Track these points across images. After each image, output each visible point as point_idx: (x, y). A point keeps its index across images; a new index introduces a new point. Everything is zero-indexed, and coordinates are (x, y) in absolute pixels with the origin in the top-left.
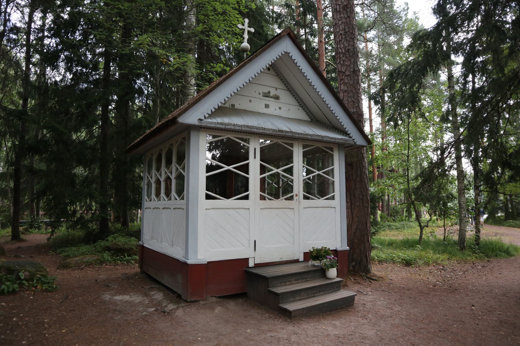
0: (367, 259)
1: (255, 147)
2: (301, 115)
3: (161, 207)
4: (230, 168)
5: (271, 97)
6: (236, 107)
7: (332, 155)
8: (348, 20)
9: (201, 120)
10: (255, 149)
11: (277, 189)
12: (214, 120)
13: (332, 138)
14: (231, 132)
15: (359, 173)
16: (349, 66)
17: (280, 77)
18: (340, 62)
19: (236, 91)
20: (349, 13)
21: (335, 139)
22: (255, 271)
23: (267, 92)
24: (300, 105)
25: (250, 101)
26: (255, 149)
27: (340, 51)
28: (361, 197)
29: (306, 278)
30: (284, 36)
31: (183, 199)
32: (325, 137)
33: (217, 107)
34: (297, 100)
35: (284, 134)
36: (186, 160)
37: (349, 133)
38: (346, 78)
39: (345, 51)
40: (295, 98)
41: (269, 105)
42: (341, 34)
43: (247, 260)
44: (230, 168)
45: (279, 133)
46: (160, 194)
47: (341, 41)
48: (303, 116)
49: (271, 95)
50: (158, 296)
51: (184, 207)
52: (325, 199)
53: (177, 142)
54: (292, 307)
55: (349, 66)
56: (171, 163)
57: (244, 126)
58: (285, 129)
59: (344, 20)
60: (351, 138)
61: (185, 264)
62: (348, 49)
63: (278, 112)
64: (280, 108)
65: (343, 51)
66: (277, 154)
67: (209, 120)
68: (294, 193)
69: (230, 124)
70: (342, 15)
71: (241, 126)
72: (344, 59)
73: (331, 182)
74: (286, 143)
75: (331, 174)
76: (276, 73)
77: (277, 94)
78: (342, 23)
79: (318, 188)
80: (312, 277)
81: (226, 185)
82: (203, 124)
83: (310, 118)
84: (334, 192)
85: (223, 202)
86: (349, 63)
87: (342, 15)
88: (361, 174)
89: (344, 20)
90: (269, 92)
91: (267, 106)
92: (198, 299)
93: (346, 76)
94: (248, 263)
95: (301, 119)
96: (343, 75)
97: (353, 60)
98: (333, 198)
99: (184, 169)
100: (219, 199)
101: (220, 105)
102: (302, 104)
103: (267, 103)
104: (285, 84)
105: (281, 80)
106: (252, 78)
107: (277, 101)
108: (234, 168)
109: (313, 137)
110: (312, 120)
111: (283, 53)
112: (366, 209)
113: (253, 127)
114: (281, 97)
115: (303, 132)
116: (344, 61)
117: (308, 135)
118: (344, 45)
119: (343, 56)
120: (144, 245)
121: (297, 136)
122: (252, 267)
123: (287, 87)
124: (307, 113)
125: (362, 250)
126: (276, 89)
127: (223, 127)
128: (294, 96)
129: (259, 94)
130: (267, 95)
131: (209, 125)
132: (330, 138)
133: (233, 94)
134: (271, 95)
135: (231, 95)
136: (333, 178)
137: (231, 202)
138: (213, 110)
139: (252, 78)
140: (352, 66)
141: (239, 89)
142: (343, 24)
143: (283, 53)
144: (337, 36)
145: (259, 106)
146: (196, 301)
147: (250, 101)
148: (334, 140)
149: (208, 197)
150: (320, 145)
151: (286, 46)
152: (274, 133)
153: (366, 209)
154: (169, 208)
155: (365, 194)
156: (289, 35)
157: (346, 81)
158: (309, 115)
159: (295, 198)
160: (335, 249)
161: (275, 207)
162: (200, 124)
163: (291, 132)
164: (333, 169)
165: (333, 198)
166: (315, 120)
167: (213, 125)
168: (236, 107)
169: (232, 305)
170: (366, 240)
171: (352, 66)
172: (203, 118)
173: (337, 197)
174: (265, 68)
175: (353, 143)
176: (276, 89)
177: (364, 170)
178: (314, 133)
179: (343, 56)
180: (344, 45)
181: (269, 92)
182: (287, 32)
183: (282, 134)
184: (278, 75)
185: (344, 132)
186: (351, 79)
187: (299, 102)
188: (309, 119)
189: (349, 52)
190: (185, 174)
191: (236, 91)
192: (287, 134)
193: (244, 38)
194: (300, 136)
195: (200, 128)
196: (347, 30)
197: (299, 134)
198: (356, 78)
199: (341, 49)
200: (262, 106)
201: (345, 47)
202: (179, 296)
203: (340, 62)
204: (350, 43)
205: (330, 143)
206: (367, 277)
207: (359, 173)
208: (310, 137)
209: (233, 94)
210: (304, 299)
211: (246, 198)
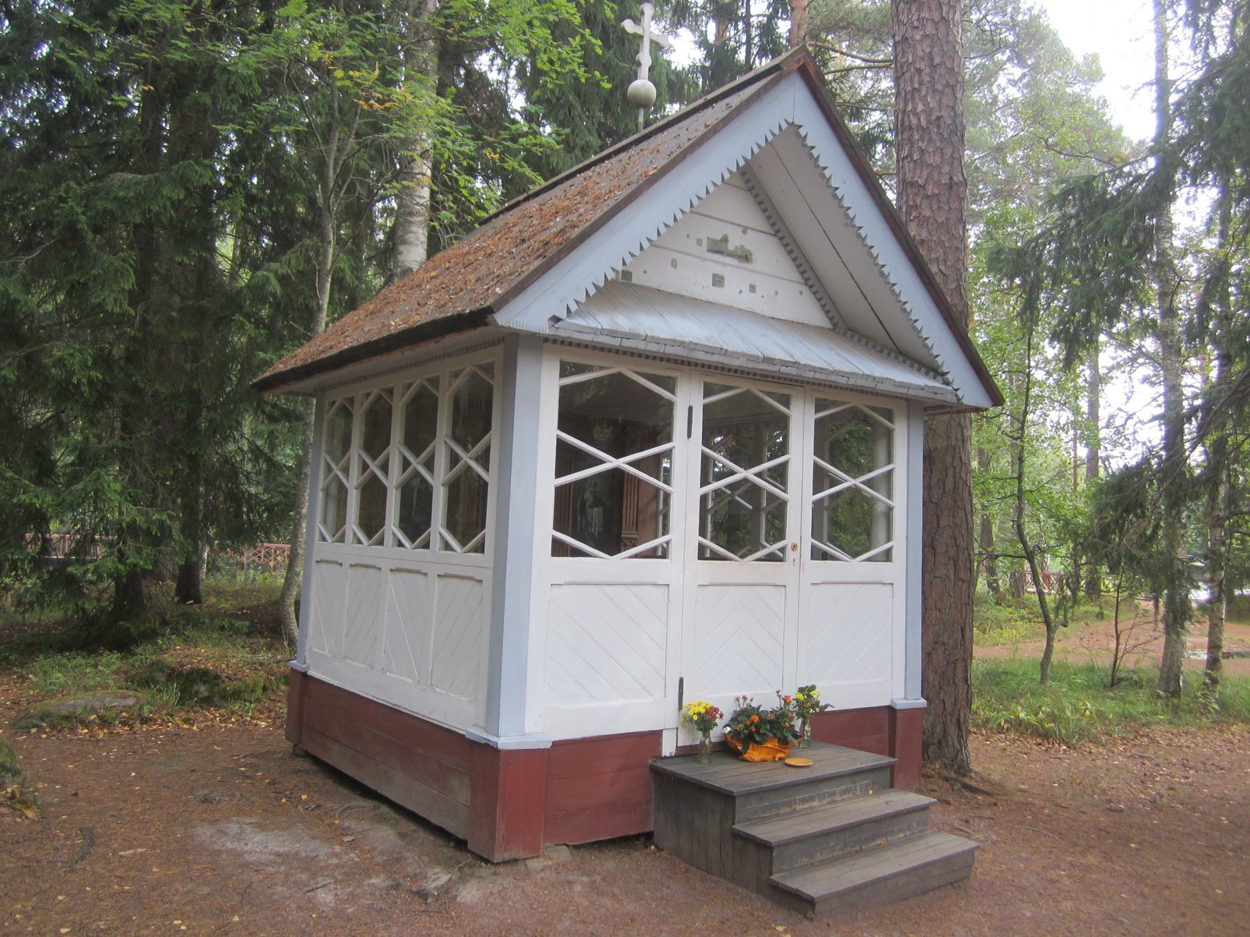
0: (960, 729)
1: (688, 402)
2: (806, 309)
3: (386, 566)
4: (622, 463)
5: (730, 255)
6: (634, 281)
7: (889, 434)
8: (942, 28)
9: (556, 319)
10: (690, 409)
11: (739, 526)
12: (590, 323)
13: (902, 385)
14: (627, 357)
15: (949, 486)
16: (938, 167)
17: (756, 196)
18: (910, 155)
19: (654, 237)
20: (945, 8)
21: (909, 386)
22: (686, 770)
23: (719, 237)
24: (807, 280)
25: (674, 264)
26: (690, 409)
27: (914, 121)
28: (952, 552)
29: (834, 794)
30: (789, 73)
31: (480, 548)
32: (882, 380)
33: (601, 284)
34: (798, 266)
35: (776, 368)
36: (494, 436)
37: (945, 369)
38: (925, 203)
39: (929, 122)
40: (794, 260)
41: (723, 278)
42: (919, 71)
43: (656, 735)
44: (622, 463)
45: (764, 366)
46: (381, 523)
47: (918, 90)
48: (811, 313)
49: (731, 247)
50: (385, 835)
51: (487, 576)
52: (869, 560)
53: (457, 374)
54: (815, 884)
55: (938, 167)
56: (433, 435)
57: (674, 343)
58: (779, 354)
59: (929, 29)
60: (948, 384)
61: (487, 750)
62: (938, 118)
63: (745, 301)
64: (752, 288)
65: (924, 123)
66: (745, 425)
67: (579, 321)
68: (788, 542)
69: (635, 336)
70: (925, 14)
71: (665, 342)
72: (923, 145)
73: (880, 508)
74: (769, 394)
75: (883, 487)
76: (747, 181)
77: (748, 247)
78: (925, 36)
79: (848, 527)
80: (847, 791)
81: (605, 517)
82: (563, 333)
83: (831, 319)
84: (889, 538)
85: (599, 564)
86: (938, 159)
87: (925, 14)
88: (955, 487)
89: (929, 29)
90: (725, 240)
91: (718, 281)
92: (519, 854)
93: (928, 197)
94: (660, 744)
95: (806, 321)
96: (916, 194)
97: (948, 151)
98: (887, 556)
99: (484, 459)
100: (595, 557)
101: (611, 276)
102: (810, 277)
103: (720, 270)
104: (769, 218)
105: (760, 203)
106: (699, 198)
107: (744, 265)
108: (632, 464)
109: (852, 381)
110: (835, 325)
111: (784, 126)
112: (965, 585)
113: (694, 346)
114: (756, 255)
115: (825, 366)
116: (922, 151)
117: (838, 373)
118: (926, 104)
119: (922, 139)
120: (311, 673)
121: (810, 375)
122: (671, 757)
123: (773, 225)
124: (823, 306)
125: (949, 707)
126: (745, 232)
127: (615, 342)
128: (790, 252)
129: (699, 242)
130: (718, 247)
131: (577, 336)
132: (894, 383)
133: (646, 245)
134: (731, 247)
135: (642, 248)
136: (890, 496)
137: (621, 564)
138: (592, 291)
139: (699, 198)
140: (946, 169)
141: (663, 230)
142: (928, 41)
143: (784, 126)
144: (907, 76)
145: (693, 277)
146: (516, 860)
147: (674, 264)
148: (905, 391)
149: (559, 549)
150: (861, 403)
151: (792, 104)
152: (751, 365)
153: (965, 585)
154: (418, 572)
155: (963, 545)
156: (803, 72)
157: (927, 213)
158: (827, 313)
159: (790, 554)
160: (888, 703)
161: (736, 581)
162: (553, 332)
163: (796, 364)
164: (890, 473)
165: (887, 556)
166: (844, 327)
167: (587, 338)
168: (634, 281)
169: (609, 863)
170: (960, 675)
171: (946, 169)
172: (562, 314)
173: (899, 554)
174: (734, 170)
175: (954, 400)
176: (745, 232)
177: (963, 475)
178: (856, 370)
179: (922, 139)
180: (926, 104)
181: (725, 240)
182: (799, 60)
183: (771, 368)
184: (750, 190)
185: (933, 370)
186: (939, 208)
187: (802, 273)
188: (826, 324)
189: (939, 127)
190: (490, 477)
191: (654, 237)
192: (783, 369)
193: (639, 64)
194: (818, 376)
195: (539, 343)
196: (937, 60)
197: (814, 369)
198: (954, 205)
199: (917, 115)
200: (686, 273)
201: (928, 112)
202: (461, 844)
203: (910, 155)
204: (944, 100)
205: (887, 396)
206: (965, 786)
207: (949, 486)
208: (843, 381)
209: (646, 245)
210: (836, 859)
211: (661, 553)
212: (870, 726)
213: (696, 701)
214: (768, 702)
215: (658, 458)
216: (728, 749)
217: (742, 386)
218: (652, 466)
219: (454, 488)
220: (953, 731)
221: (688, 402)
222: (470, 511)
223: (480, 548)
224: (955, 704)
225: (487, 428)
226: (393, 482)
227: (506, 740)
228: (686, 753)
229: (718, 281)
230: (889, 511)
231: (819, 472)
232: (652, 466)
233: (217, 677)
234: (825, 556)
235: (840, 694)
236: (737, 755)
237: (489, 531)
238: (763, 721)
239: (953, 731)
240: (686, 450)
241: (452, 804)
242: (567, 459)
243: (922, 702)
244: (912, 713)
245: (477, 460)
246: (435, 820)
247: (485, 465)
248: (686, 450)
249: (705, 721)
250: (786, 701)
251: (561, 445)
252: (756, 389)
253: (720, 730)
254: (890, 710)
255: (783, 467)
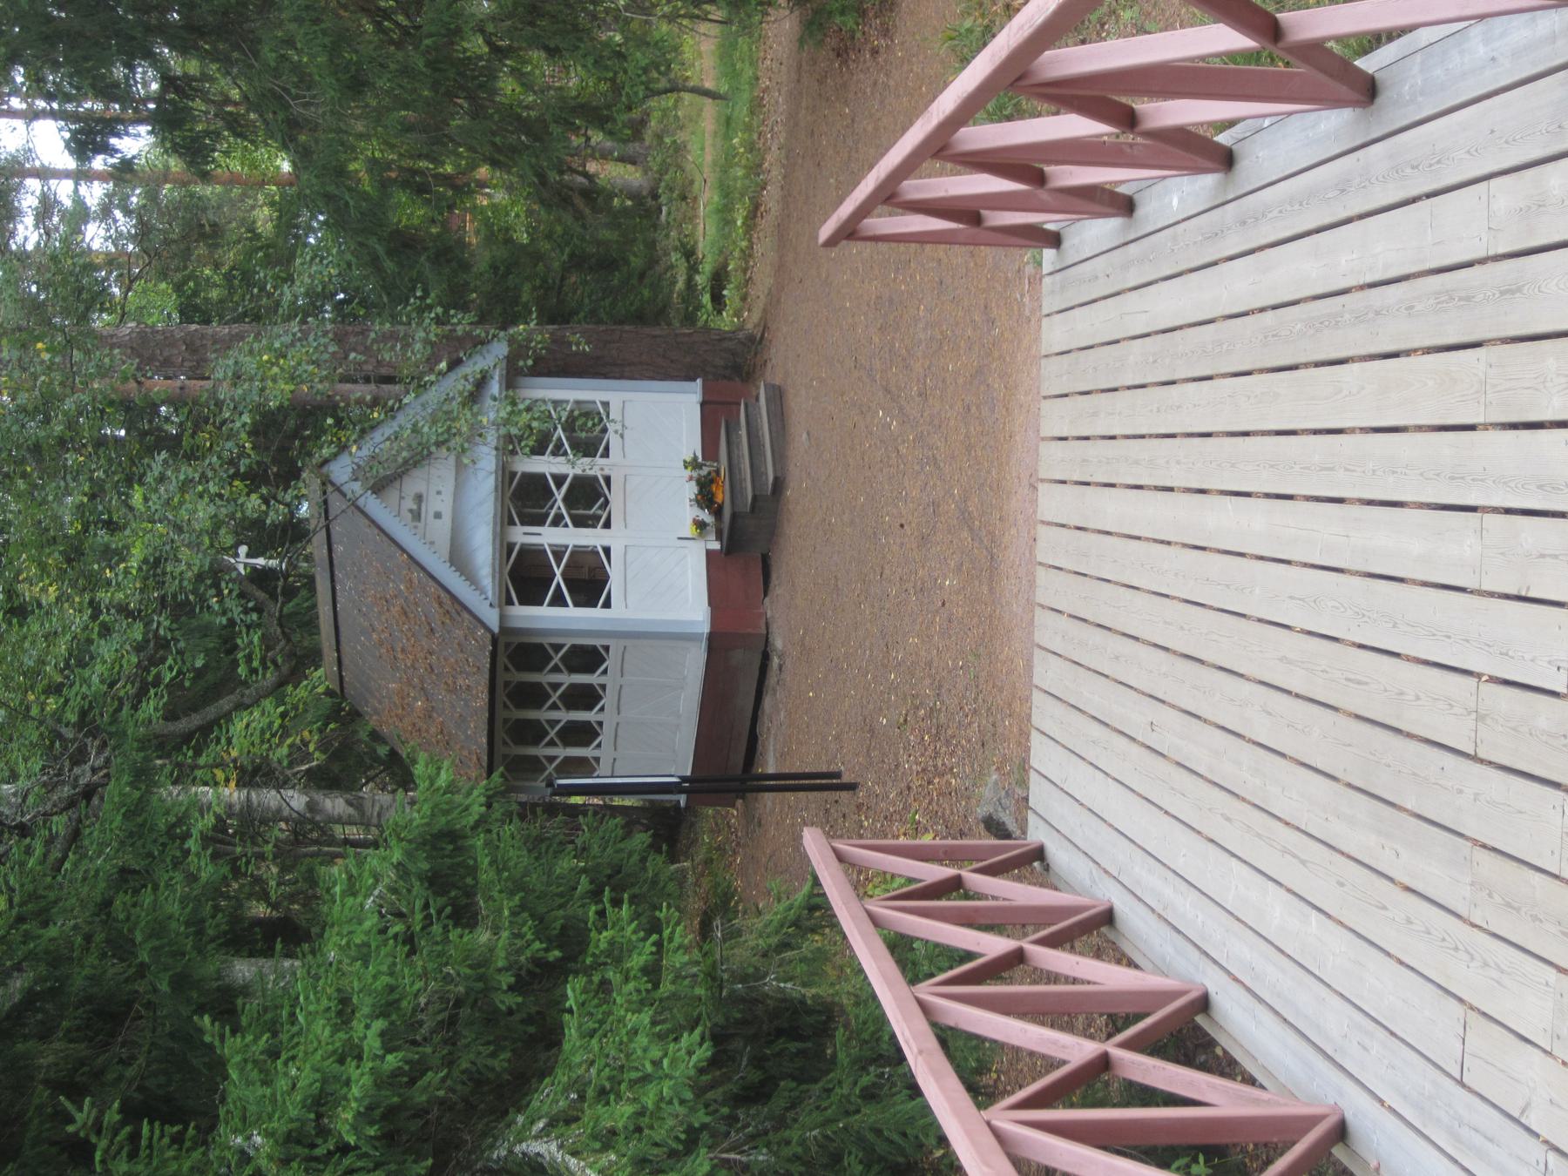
1: (521, 535)
11: (588, 499)
36: (545, 641)
43: (709, 553)
51: (622, 642)
61: (712, 637)
64: (439, 493)
81: (589, 582)
85: (615, 585)
90: (411, 511)
91: (438, 515)
98: (606, 405)
99: (557, 648)
103: (431, 514)
130: (417, 515)
137: (615, 572)
149: (607, 605)
159: (606, 472)
165: (606, 405)
181: (411, 511)
185: (840, 857)
190: (569, 642)
195: (502, 617)
211: (607, 551)
212: (715, 418)
213: (689, 530)
214: (691, 490)
215: (554, 553)
216: (718, 512)
217: (508, 501)
218: (558, 555)
219: (572, 670)
220: (726, 344)
221: (521, 535)
222: (588, 657)
223: (607, 648)
224: (706, 343)
225: (541, 646)
226: (565, 716)
227: (706, 629)
228: (719, 537)
229: (438, 515)
230: (577, 402)
231: (555, 453)
232: (558, 555)
233: (705, 913)
234: (607, 448)
235: (690, 442)
236: (721, 507)
237: (598, 642)
238: (700, 492)
239: (726, 344)
240: (548, 537)
241: (745, 660)
242: (559, 601)
243: (699, 381)
244: (706, 390)
245: (557, 652)
246: (757, 673)
247: (562, 646)
248: (548, 537)
249: (700, 525)
250: (691, 478)
251: (551, 604)
252: (509, 494)
253: (706, 516)
254: (703, 404)
255: (554, 477)
